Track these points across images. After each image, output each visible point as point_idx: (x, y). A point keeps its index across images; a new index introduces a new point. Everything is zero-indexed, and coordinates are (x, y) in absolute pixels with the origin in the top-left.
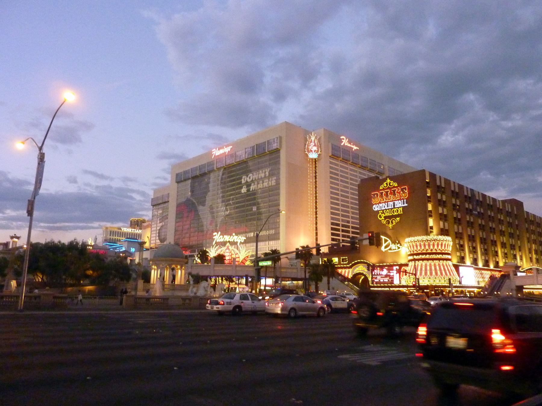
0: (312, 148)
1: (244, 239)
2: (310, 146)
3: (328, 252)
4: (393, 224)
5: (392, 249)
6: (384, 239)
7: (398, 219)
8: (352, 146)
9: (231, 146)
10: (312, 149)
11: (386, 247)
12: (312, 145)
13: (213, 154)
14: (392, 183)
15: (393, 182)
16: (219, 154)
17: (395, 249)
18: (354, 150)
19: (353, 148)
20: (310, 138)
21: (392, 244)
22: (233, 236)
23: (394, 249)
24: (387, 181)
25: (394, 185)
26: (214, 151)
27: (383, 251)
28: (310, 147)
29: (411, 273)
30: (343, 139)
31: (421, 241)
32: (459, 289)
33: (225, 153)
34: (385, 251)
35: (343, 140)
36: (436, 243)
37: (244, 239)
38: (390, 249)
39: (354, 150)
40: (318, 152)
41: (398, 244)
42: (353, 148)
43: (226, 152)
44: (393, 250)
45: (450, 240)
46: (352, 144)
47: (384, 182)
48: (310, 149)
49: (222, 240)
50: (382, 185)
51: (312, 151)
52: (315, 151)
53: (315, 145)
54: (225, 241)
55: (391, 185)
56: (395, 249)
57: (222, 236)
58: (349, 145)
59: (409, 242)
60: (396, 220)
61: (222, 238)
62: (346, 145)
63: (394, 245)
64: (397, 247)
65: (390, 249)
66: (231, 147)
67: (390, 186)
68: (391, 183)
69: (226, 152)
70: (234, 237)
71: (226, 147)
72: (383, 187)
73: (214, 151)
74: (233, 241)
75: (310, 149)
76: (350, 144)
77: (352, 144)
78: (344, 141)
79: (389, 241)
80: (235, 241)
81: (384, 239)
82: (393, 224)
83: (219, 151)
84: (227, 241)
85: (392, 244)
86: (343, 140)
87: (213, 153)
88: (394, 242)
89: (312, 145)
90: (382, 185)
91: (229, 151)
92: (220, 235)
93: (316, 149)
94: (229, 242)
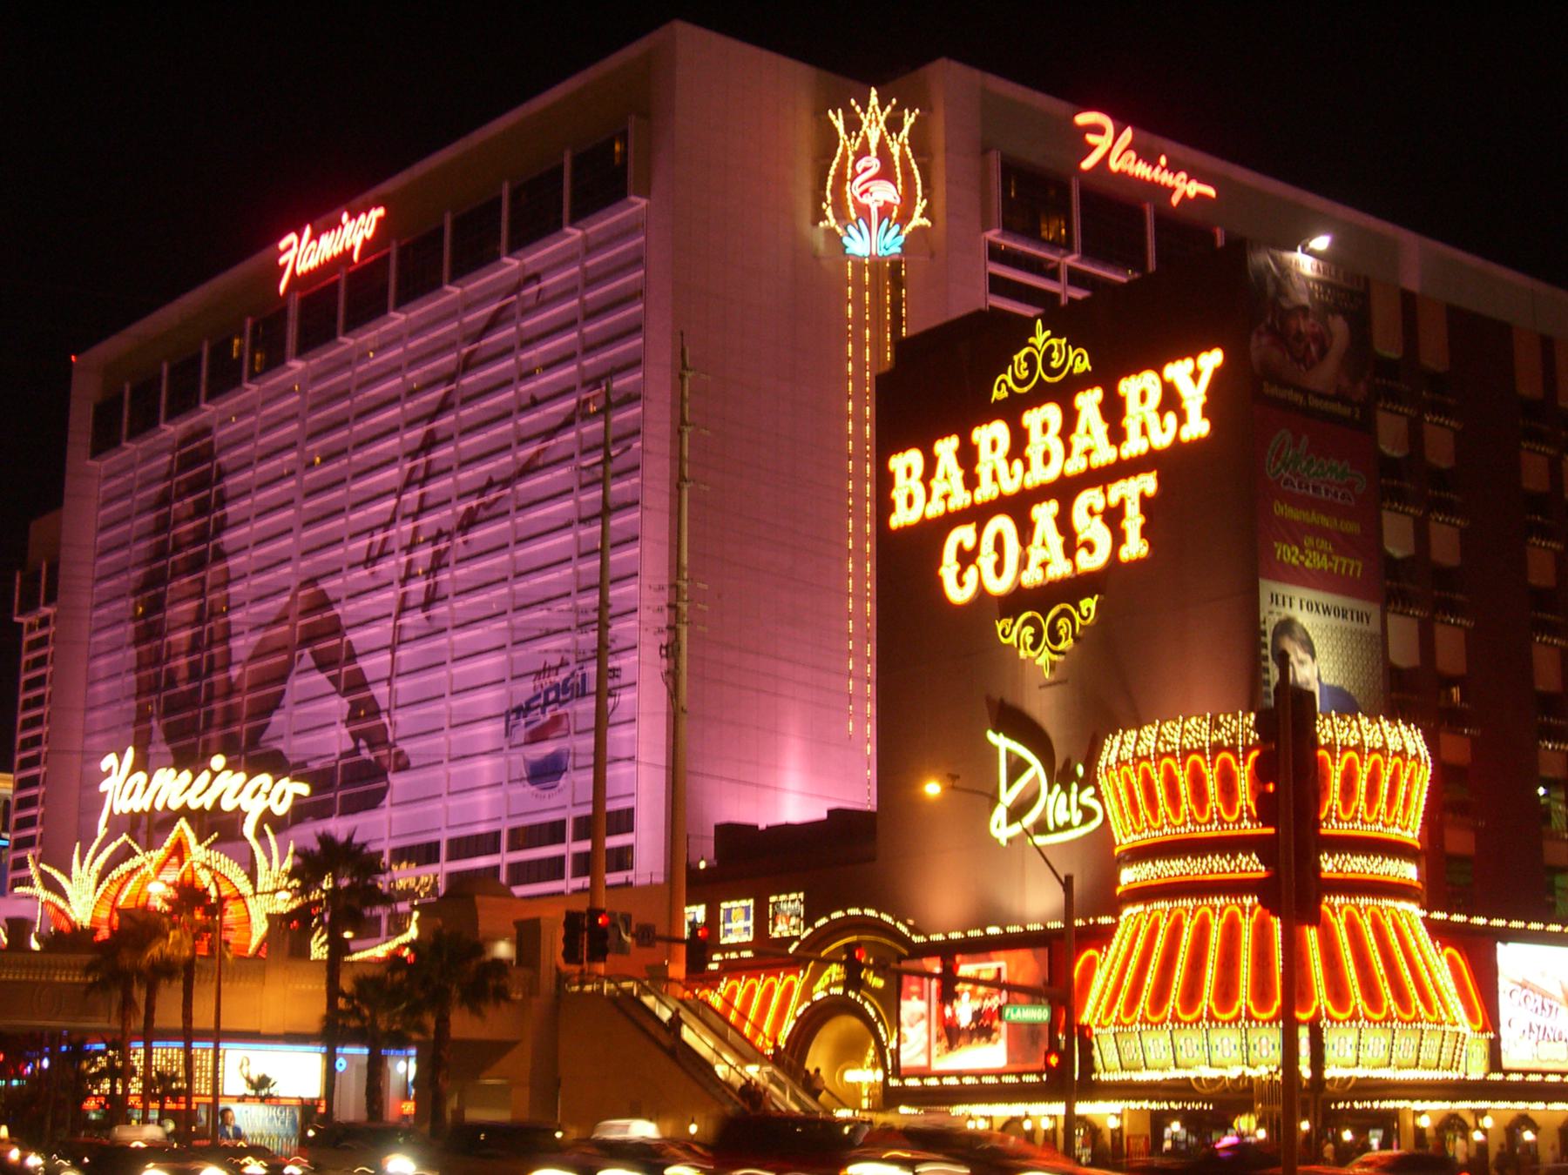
0: (866, 191)
1: (297, 797)
2: (855, 175)
3: (1499, 945)
4: (1062, 646)
5: (1051, 826)
6: (1009, 753)
7: (1089, 604)
8: (1166, 178)
9: (377, 207)
10: (865, 200)
11: (1015, 814)
12: (865, 170)
13: (286, 265)
14: (1060, 351)
15: (1064, 341)
16: (313, 263)
17: (1068, 826)
18: (1175, 200)
19: (1174, 189)
20: (853, 125)
21: (1050, 791)
22: (215, 775)
23: (1060, 823)
24: (1031, 340)
25: (1070, 363)
26: (290, 247)
27: (997, 840)
28: (852, 190)
29: (661, 939)
30: (1099, 130)
31: (1201, 751)
32: (1539, 1106)
33: (347, 254)
34: (1010, 841)
35: (1091, 138)
36: (1367, 768)
37: (297, 797)
38: (1041, 827)
39: (1175, 200)
40: (905, 218)
41: (1082, 786)
42: (1174, 189)
43: (353, 248)
44: (1058, 829)
45: (1411, 751)
46: (1163, 160)
47: (1017, 352)
48: (855, 200)
49: (140, 804)
50: (1006, 373)
51: (864, 212)
52: (885, 211)
53: (886, 174)
54: (159, 806)
55: (1055, 364)
56: (1068, 826)
57: (141, 777)
58: (1142, 170)
59: (1126, 763)
60: (1076, 615)
61: (140, 788)
62: (1114, 165)
63: (1063, 795)
64: (1080, 806)
65: (1041, 827)
66: (380, 212)
67: (1050, 371)
68: (1055, 355)
69: (353, 248)
70: (219, 778)
71: (350, 219)
72: (1011, 383)
73: (290, 247)
74: (208, 807)
75: (855, 200)
76: (1153, 163)
77: (1163, 160)
78: (1102, 143)
79: (1036, 768)
80: (228, 805)
81: (1009, 753)
82: (1062, 646)
83: (314, 244)
84: (175, 805)
85: (1050, 791)
86: (1091, 138)
87: (282, 261)
88: (1062, 777)
89: (865, 170)
90: (1006, 373)
91: (365, 240)
92: (133, 771)
93: (891, 200)
94: (185, 811)
